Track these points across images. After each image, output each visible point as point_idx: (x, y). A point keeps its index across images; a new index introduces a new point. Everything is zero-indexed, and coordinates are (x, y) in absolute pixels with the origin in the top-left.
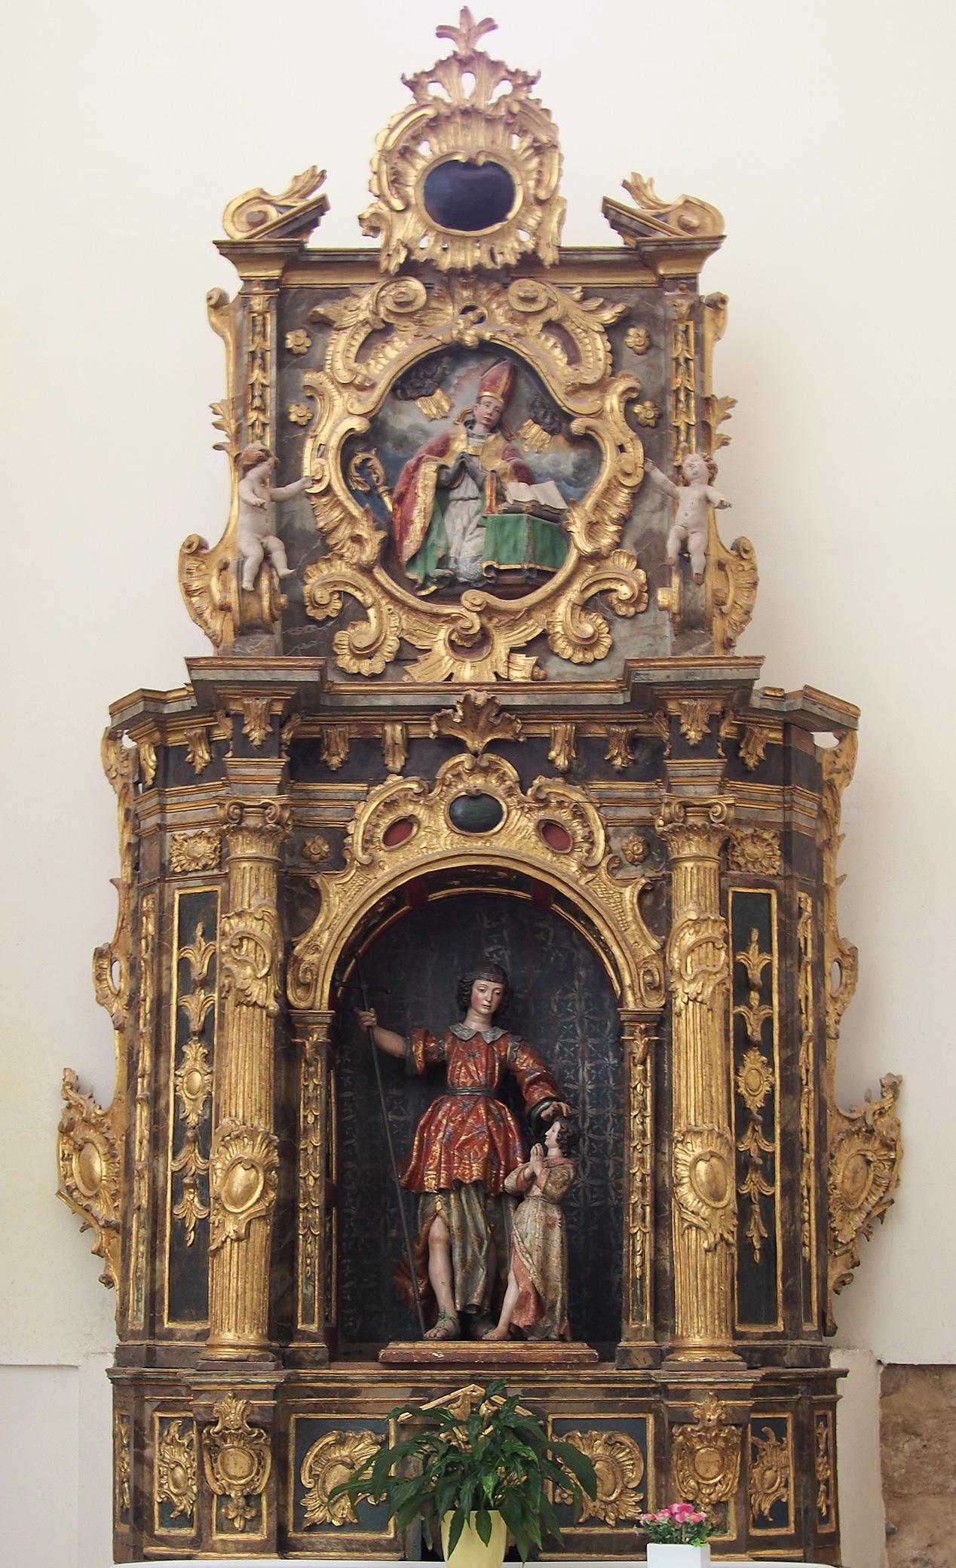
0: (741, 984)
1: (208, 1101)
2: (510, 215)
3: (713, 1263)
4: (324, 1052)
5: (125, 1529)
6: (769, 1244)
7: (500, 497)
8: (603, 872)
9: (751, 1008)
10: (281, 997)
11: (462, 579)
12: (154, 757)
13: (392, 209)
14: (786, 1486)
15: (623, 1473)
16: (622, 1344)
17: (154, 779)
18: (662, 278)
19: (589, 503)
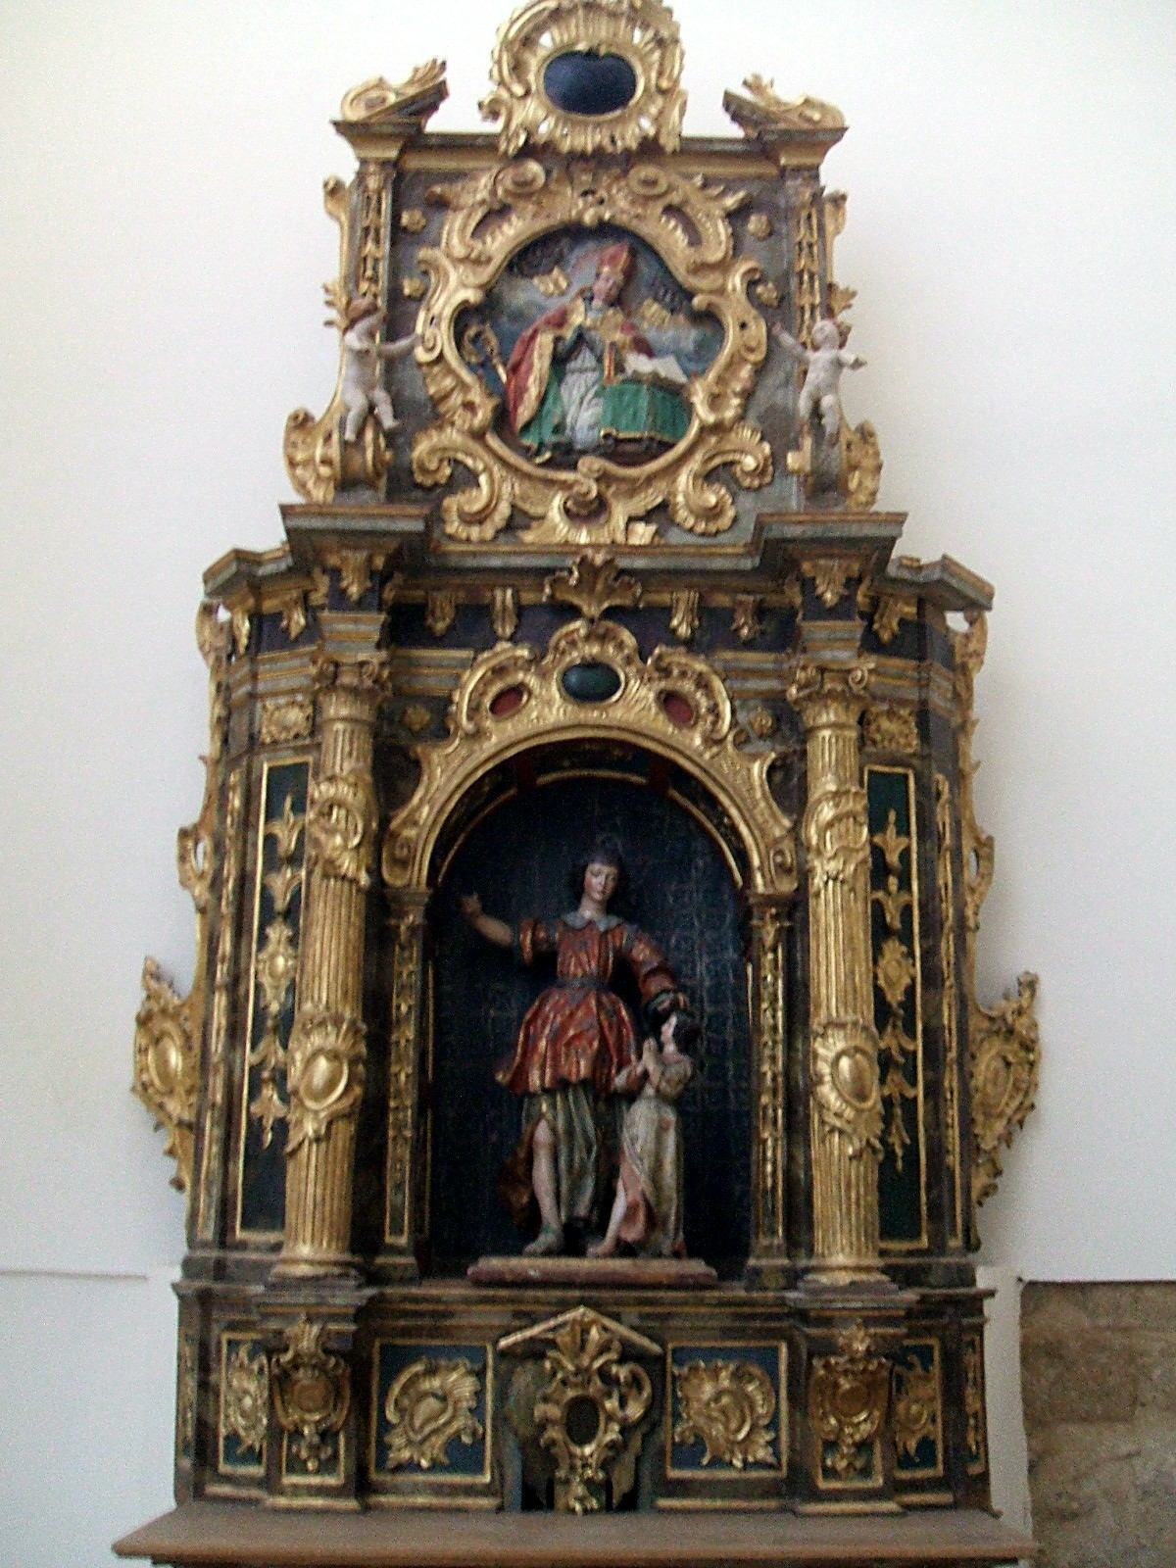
0: (879, 870)
1: (292, 988)
2: (632, 102)
3: (858, 1171)
4: (420, 933)
5: (187, 1463)
6: (911, 1152)
7: (619, 367)
8: (730, 747)
9: (889, 894)
10: (375, 871)
11: (578, 447)
12: (247, 624)
13: (512, 95)
14: (934, 1420)
15: (752, 1408)
16: (752, 1262)
17: (247, 648)
18: (783, 171)
19: (711, 376)
